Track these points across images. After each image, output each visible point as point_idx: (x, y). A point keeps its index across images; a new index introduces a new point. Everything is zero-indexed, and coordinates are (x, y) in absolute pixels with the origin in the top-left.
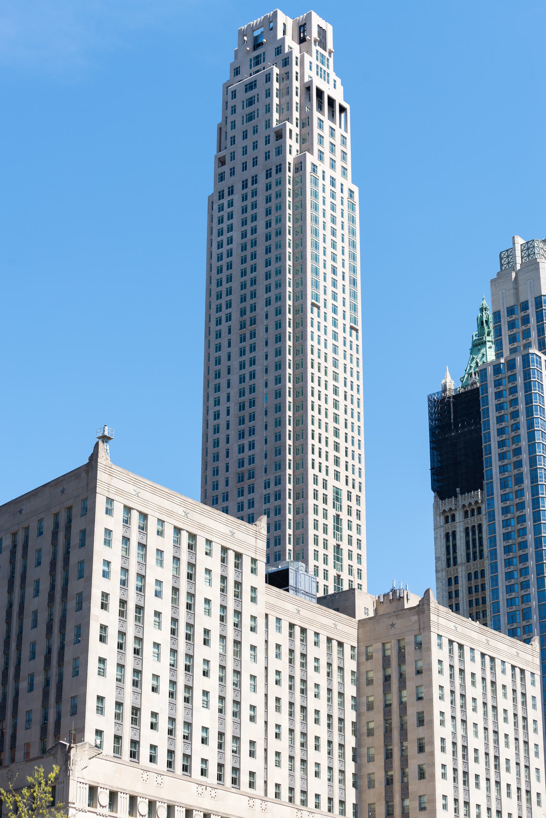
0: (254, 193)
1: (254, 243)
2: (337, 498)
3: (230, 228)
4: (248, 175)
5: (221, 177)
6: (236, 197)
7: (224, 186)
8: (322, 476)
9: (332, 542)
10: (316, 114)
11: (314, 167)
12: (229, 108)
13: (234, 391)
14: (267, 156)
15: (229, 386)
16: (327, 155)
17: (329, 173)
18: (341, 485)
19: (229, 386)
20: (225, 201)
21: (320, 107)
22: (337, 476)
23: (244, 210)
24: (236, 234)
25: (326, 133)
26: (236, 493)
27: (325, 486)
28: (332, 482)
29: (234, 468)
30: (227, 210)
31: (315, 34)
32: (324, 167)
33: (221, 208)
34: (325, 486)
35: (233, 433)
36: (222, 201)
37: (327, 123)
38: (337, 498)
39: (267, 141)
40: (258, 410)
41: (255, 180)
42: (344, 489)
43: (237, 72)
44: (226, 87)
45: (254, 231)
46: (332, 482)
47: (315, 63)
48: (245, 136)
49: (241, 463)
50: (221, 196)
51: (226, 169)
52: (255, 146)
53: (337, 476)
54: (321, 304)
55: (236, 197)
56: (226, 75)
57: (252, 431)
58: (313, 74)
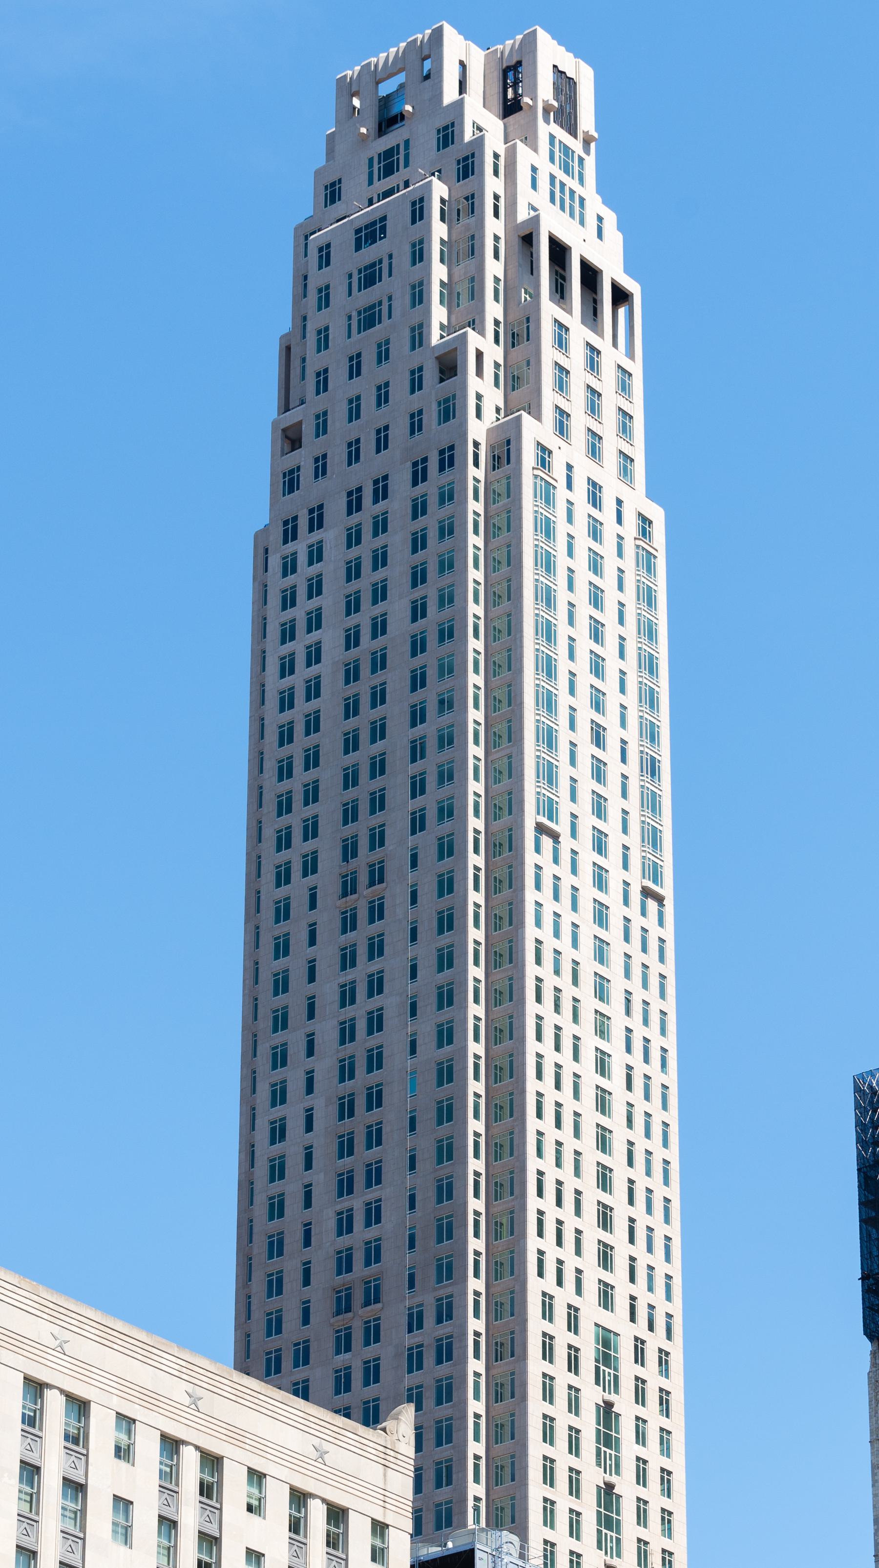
0: (381, 525)
1: (380, 662)
2: (606, 1356)
3: (315, 621)
4: (363, 475)
5: (290, 482)
6: (332, 536)
7: (298, 505)
8: (564, 1297)
9: (593, 1477)
10: (549, 310)
11: (544, 454)
12: (311, 294)
13: (325, 1066)
14: (416, 424)
15: (310, 1052)
16: (579, 421)
17: (584, 469)
18: (617, 1320)
19: (310, 1052)
20: (300, 547)
21: (560, 291)
22: (606, 1296)
23: (353, 571)
24: (330, 638)
25: (576, 360)
26: (330, 1345)
27: (573, 1325)
28: (591, 1313)
29: (324, 1276)
30: (305, 571)
31: (545, 90)
32: (569, 452)
33: (289, 566)
34: (573, 1325)
35: (322, 1180)
36: (291, 547)
37: (580, 333)
38: (606, 1356)
39: (416, 384)
40: (391, 1115)
41: (381, 490)
42: (626, 1333)
43: (332, 193)
44: (304, 234)
45: (380, 627)
46: (591, 1313)
47: (546, 168)
48: (355, 369)
49: (344, 1263)
50: (290, 533)
51: (304, 458)
52: (383, 396)
53: (606, 1296)
54: (562, 827)
55: (332, 536)
56: (304, 203)
57: (374, 1175)
58: (541, 198)
